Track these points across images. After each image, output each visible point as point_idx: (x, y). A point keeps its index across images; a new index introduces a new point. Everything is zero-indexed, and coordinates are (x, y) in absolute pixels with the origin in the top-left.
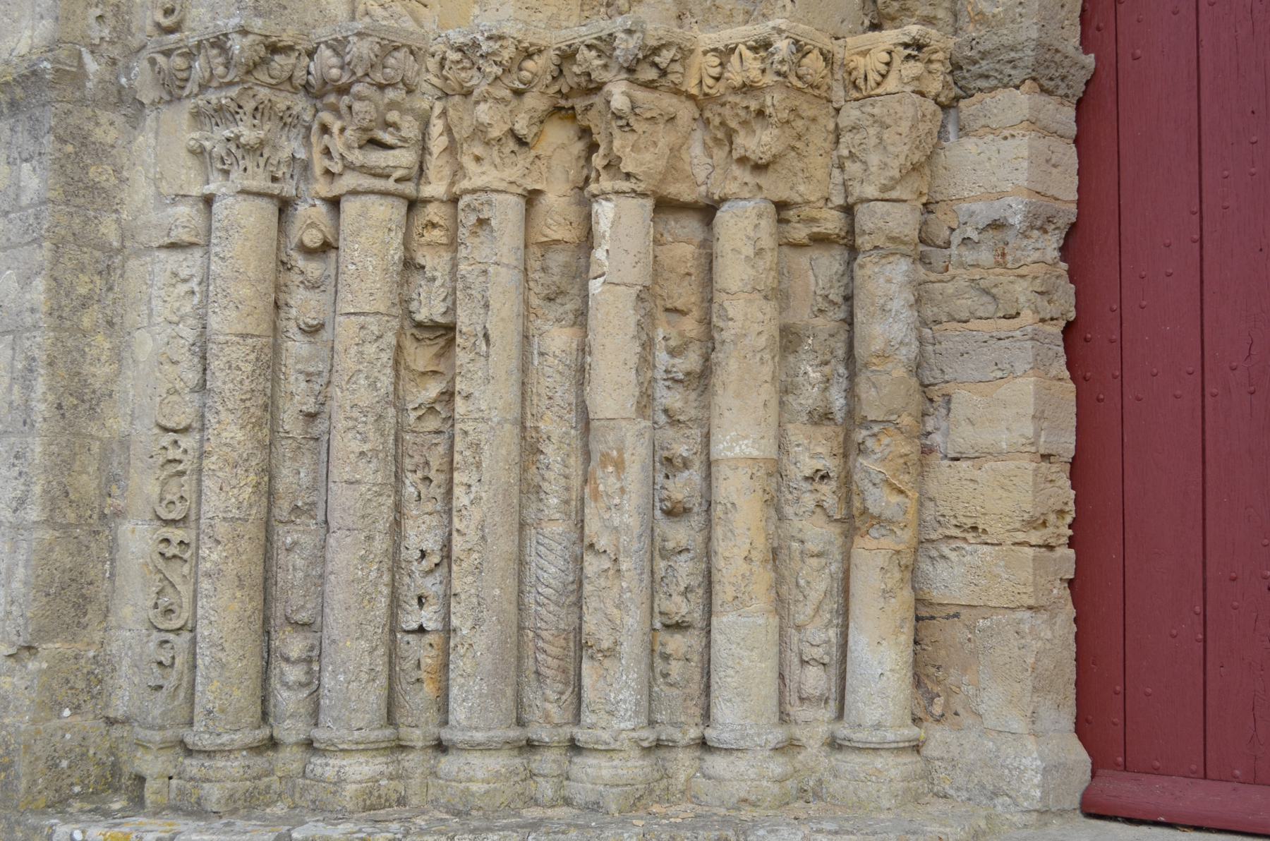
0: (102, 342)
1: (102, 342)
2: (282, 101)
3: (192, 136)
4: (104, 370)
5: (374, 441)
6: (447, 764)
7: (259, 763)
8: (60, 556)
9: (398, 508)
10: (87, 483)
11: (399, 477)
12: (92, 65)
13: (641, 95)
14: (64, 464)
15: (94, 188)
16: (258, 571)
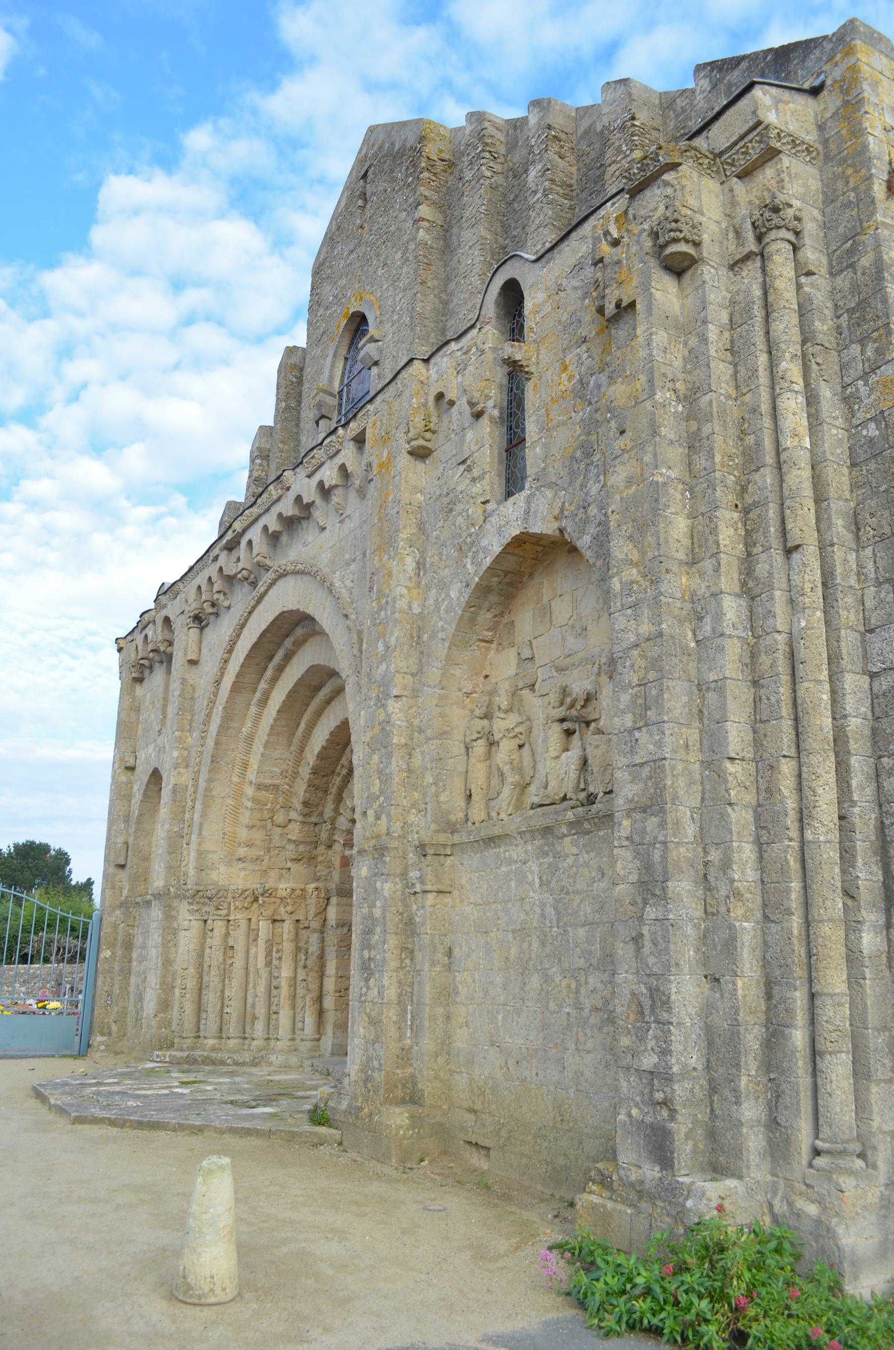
0: (173, 949)
1: (173, 949)
2: (202, 900)
3: (187, 907)
4: (173, 956)
5: (218, 972)
6: (228, 1041)
7: (196, 1040)
8: (163, 996)
9: (224, 986)
10: (169, 980)
11: (224, 980)
12: (172, 890)
13: (265, 899)
14: (164, 976)
15: (172, 916)
16: (197, 1000)
